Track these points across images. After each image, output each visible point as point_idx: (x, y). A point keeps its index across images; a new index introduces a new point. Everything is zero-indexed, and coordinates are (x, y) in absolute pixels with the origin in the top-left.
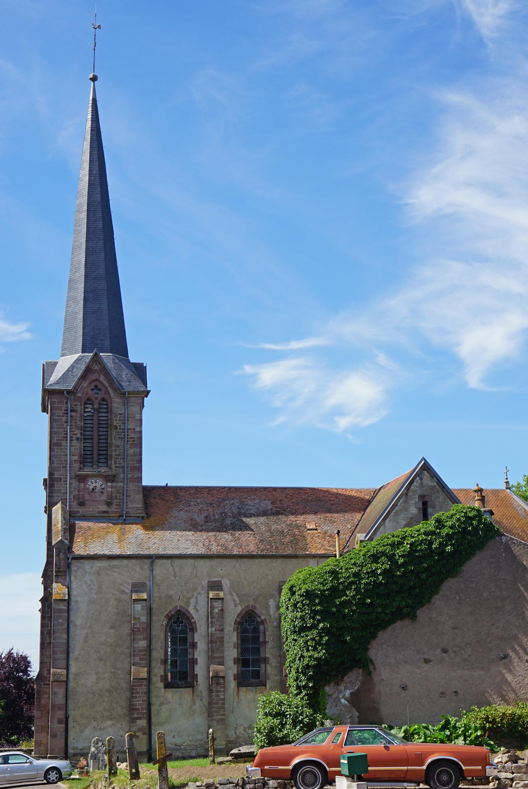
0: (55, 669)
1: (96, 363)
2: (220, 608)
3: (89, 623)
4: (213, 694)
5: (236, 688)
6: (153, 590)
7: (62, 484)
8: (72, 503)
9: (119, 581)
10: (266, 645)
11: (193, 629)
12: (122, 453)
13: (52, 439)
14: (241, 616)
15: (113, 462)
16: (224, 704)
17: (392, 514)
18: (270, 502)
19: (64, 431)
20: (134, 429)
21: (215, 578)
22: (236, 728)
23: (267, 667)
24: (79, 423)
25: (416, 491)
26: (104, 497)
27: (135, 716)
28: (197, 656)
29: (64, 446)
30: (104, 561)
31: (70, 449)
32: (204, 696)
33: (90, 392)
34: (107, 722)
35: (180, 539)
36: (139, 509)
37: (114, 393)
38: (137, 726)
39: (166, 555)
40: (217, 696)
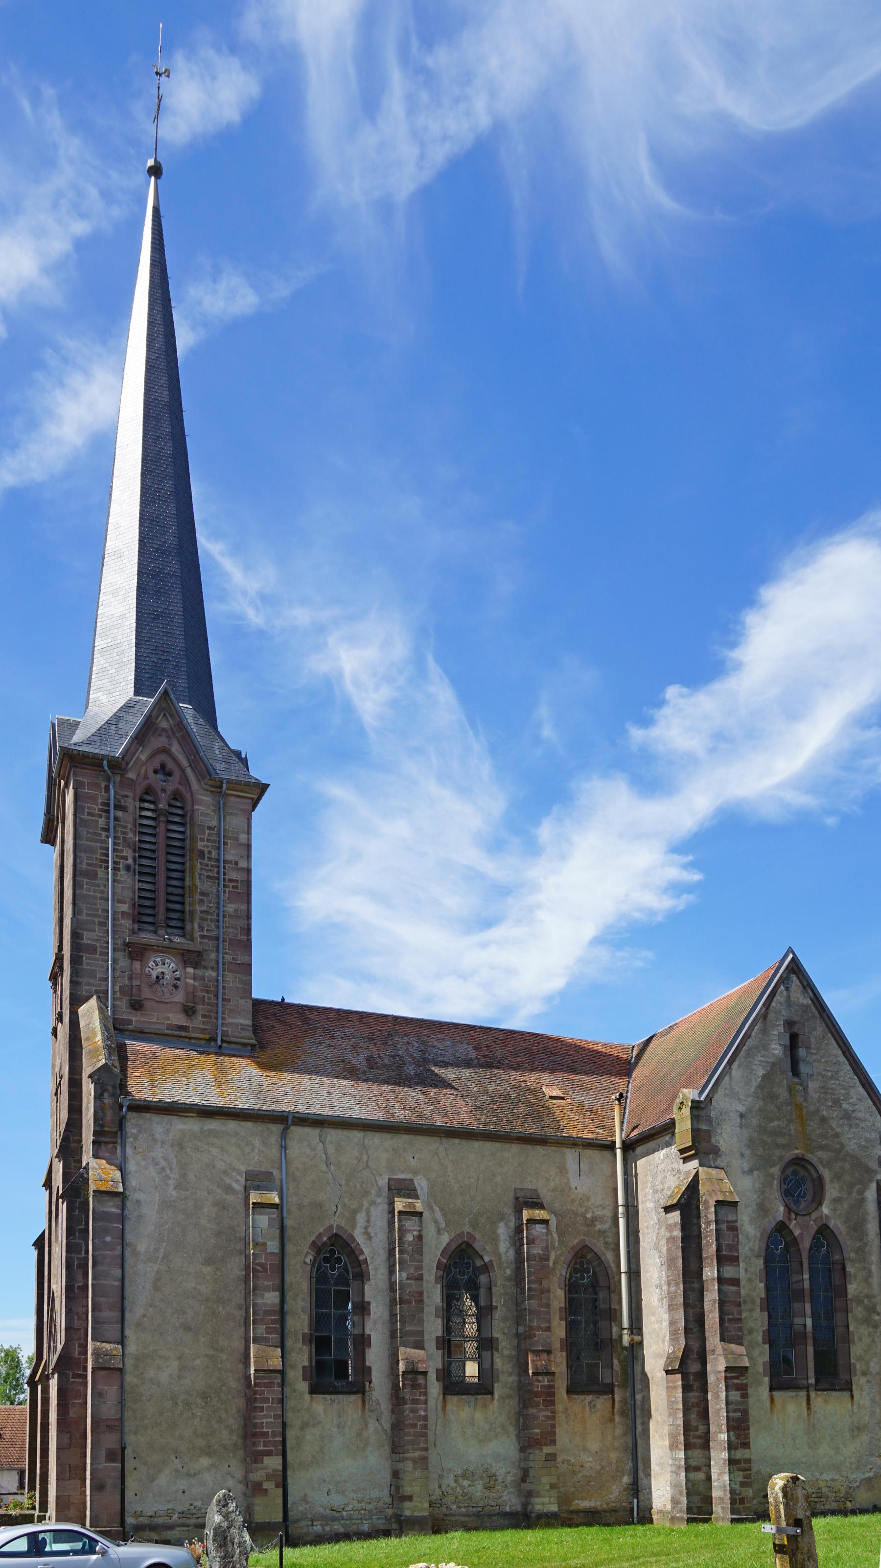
0: (98, 1344)
1: (165, 715)
2: (416, 1233)
3: (162, 1250)
4: (406, 1406)
5: (441, 1396)
6: (288, 1189)
7: (98, 960)
8: (118, 1003)
9: (221, 1165)
10: (493, 1313)
11: (362, 1276)
12: (213, 909)
13: (78, 860)
14: (450, 1253)
15: (196, 926)
16: (425, 1427)
17: (742, 1053)
18: (471, 1047)
19: (101, 848)
20: (236, 863)
21: (402, 1172)
22: (441, 1477)
23: (494, 1357)
24: (130, 835)
25: (780, 1011)
26: (179, 997)
27: (261, 1448)
28: (371, 1330)
29: (101, 879)
30: (191, 1121)
31: (113, 887)
32: (384, 1411)
33: (151, 773)
34: (201, 1459)
35: (332, 1091)
36: (246, 1030)
37: (199, 781)
38: (262, 1469)
39: (314, 1117)
40: (414, 1411)
